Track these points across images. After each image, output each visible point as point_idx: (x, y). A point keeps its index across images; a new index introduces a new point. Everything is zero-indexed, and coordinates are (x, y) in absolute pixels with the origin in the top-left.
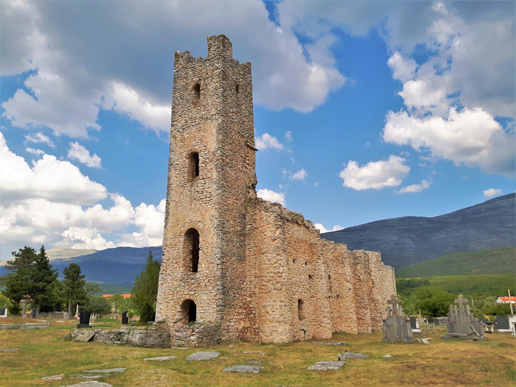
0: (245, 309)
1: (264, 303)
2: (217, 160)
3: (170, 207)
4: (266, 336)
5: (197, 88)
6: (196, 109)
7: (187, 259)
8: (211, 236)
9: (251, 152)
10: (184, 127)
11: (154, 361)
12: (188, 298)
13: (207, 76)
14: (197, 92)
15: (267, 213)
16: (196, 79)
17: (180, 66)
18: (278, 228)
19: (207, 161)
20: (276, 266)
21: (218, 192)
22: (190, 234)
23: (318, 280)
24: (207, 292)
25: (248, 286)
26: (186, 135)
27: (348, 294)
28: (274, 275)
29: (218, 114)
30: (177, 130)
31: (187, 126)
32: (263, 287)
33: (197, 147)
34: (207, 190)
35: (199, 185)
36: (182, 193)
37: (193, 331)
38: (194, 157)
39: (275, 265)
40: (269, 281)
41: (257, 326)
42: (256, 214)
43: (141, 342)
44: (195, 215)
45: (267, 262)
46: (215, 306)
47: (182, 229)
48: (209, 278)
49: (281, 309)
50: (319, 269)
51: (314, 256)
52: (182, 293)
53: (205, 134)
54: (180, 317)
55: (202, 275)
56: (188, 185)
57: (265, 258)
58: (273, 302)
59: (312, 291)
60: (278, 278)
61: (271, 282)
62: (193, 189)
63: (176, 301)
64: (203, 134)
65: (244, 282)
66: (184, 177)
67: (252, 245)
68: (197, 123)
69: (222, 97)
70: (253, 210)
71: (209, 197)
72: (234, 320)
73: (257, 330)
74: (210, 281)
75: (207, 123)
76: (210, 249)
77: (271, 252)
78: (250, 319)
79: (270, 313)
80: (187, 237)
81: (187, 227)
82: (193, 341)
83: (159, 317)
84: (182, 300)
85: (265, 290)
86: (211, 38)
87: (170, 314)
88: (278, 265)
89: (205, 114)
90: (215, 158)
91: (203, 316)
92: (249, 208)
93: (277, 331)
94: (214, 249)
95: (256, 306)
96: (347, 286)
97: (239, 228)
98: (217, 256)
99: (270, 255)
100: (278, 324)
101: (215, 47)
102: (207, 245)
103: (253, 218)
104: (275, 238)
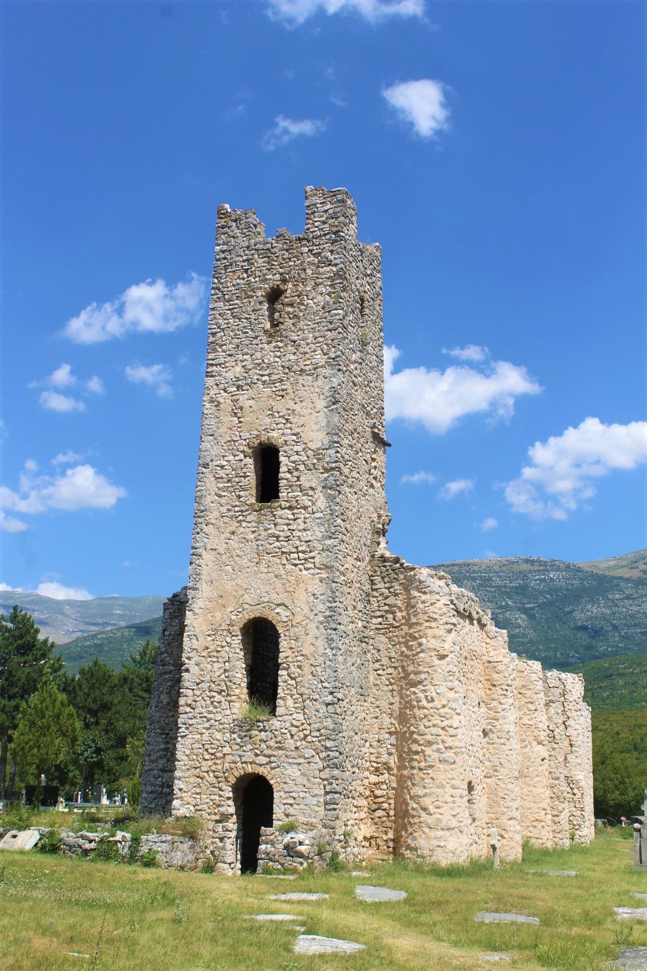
10: (240, 383)
12: (250, 771)
16: (274, 279)
22: (248, 630)
23: (502, 741)
24: (302, 760)
25: (372, 750)
27: (540, 768)
28: (441, 732)
29: (330, 365)
30: (222, 386)
33: (274, 434)
34: (299, 534)
36: (233, 533)
38: (267, 458)
39: (442, 711)
45: (424, 703)
46: (323, 792)
47: (233, 618)
53: (297, 407)
55: (288, 725)
56: (249, 518)
57: (421, 695)
58: (438, 787)
59: (487, 763)
61: (435, 747)
63: (220, 775)
64: (291, 405)
65: (366, 741)
67: (385, 661)
68: (274, 377)
70: (387, 585)
71: (304, 552)
74: (309, 739)
78: (377, 820)
79: (432, 809)
83: (180, 808)
84: (237, 774)
85: (419, 762)
91: (291, 811)
98: (325, 684)
99: (433, 688)
100: (447, 833)
102: (300, 658)
103: (387, 602)
104: (445, 653)
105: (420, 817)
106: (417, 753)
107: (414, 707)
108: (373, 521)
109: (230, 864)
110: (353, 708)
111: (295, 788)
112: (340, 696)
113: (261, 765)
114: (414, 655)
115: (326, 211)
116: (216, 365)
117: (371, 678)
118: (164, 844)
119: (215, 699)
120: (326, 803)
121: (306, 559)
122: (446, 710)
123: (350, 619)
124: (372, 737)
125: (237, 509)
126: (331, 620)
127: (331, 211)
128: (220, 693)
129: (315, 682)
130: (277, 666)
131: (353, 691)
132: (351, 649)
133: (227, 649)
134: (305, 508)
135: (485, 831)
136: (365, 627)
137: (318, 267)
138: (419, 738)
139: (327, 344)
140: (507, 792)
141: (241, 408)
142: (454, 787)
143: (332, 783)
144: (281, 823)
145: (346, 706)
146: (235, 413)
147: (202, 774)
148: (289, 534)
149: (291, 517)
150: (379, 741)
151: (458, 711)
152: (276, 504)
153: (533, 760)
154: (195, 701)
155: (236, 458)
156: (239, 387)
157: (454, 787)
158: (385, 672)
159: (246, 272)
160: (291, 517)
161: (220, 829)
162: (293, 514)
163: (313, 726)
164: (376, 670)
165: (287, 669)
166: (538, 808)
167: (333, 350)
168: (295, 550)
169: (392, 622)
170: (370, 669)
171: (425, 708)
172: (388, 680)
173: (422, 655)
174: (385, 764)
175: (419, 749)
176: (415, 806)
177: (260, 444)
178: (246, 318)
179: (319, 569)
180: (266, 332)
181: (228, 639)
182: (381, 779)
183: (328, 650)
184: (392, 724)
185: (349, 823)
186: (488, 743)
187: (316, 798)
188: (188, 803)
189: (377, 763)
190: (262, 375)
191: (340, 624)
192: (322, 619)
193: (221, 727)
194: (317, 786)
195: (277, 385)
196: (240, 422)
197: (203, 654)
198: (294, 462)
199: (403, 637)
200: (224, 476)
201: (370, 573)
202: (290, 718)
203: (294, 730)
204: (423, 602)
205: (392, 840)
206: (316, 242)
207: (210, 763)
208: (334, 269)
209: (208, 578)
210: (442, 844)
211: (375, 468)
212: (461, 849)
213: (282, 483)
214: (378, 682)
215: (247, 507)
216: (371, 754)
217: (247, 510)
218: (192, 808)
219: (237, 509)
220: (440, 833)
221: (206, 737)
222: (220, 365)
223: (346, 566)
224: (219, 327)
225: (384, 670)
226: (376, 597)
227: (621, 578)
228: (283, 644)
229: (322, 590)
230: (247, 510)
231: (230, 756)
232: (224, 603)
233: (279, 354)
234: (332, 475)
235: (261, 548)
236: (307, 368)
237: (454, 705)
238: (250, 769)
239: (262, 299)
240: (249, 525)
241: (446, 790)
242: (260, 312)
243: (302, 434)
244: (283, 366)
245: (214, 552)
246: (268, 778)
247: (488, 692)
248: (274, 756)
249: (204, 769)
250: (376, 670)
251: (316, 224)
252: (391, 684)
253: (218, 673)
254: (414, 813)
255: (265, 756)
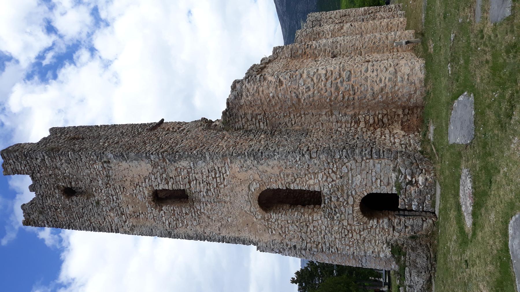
0: (375, 129)
1: (369, 96)
2: (164, 160)
3: (227, 236)
4: (415, 93)
5: (69, 192)
7: (302, 211)
8: (269, 169)
9: (163, 126)
10: (119, 213)
11: (474, 214)
12: (358, 208)
13: (53, 176)
14: (76, 194)
15: (244, 94)
17: (41, 217)
18: (265, 79)
19: (164, 176)
21: (208, 158)
23: (339, 46)
24: (350, 175)
25: (344, 126)
27: (357, 27)
28: (330, 81)
30: (123, 224)
31: (118, 208)
33: (146, 193)
34: (205, 177)
35: (198, 189)
36: (209, 217)
37: (410, 183)
39: (315, 81)
42: (245, 114)
43: (423, 273)
44: (239, 196)
45: (310, 93)
46: (371, 161)
47: (259, 217)
48: (330, 171)
50: (325, 45)
51: (307, 53)
52: (351, 216)
53: (129, 179)
54: (386, 220)
55: (326, 184)
58: (367, 81)
59: (352, 55)
61: (339, 85)
63: (362, 227)
64: (128, 183)
65: (337, 130)
66: (186, 214)
67: (287, 120)
68: (113, 193)
69: (80, 153)
71: (215, 174)
72: (392, 139)
73: (407, 111)
74: (335, 169)
75: (113, 177)
76: (289, 171)
77: (296, 87)
78: (390, 122)
79: (382, 85)
80: (270, 210)
81: (256, 208)
82: (426, 179)
84: (361, 216)
85: (350, 95)
86: (5, 170)
88: (315, 76)
89: (102, 179)
90: (160, 162)
92: (237, 126)
94: (288, 163)
96: (348, 29)
97: (262, 136)
98: (298, 159)
99: (301, 88)
100: (399, 74)
101: (17, 163)
102: (282, 176)
103: (250, 119)
105: (387, 93)
107: (313, 100)
108: (203, 129)
109: (423, 221)
110: (315, 139)
111: (370, 179)
113: (354, 201)
114: (281, 101)
115: (14, 162)
116: (111, 227)
117: (297, 128)
118: (412, 274)
119: (312, 229)
120: (379, 157)
121: (220, 172)
122: (315, 78)
124: (334, 126)
125: (193, 215)
126: (256, 155)
127: (14, 160)
128: (308, 227)
130: (288, 190)
131: (304, 140)
132: (276, 142)
133: (279, 222)
134: (188, 173)
136: (265, 133)
137: (47, 167)
138: (334, 95)
139: (90, 161)
140: (370, 41)
141: (134, 212)
142: (367, 70)
143: (365, 154)
144: (394, 188)
145: (312, 144)
146: (138, 216)
147: (362, 239)
148: (205, 183)
149: (195, 182)
150: (337, 122)
151: (315, 71)
152: (188, 191)
154: (314, 242)
155: (163, 215)
157: (367, 70)
158: (293, 119)
159: (57, 209)
161: (399, 228)
162: (193, 181)
163: (326, 167)
164: (292, 125)
165: (289, 184)
167: (92, 157)
168: (215, 180)
169: (262, 116)
170: (291, 129)
171: (314, 93)
172: (298, 117)
173: (280, 96)
174: (352, 118)
175: (341, 95)
176: (380, 96)
177: (153, 201)
178: (82, 209)
180: (88, 199)
182: (362, 120)
183: (276, 157)
184: (326, 114)
186: (340, 55)
187: (376, 165)
188: (382, 248)
189: (352, 122)
190: (113, 200)
191: (259, 150)
192: (256, 162)
193: (330, 226)
195: (117, 191)
196: (142, 213)
197: (284, 236)
198: (162, 180)
199: (270, 109)
200: (175, 222)
202: (321, 182)
203: (329, 180)
204: (247, 96)
205: (403, 111)
207: (355, 234)
209: (237, 233)
210: (406, 77)
211: (173, 128)
212: (410, 64)
214: (300, 124)
215: (192, 209)
216: (346, 127)
217: (193, 208)
219: (193, 215)
220: (399, 79)
222: (111, 225)
223: (224, 146)
225: (292, 120)
226: (248, 126)
227: (289, 26)
228: (274, 186)
229: (238, 162)
230: (193, 208)
231: (349, 221)
232: (251, 223)
233: (100, 190)
234: (166, 156)
235: (215, 200)
236: (105, 173)
237: (312, 73)
238: (357, 208)
239: (70, 200)
240: (202, 207)
242: (78, 201)
243: (144, 176)
244: (106, 188)
245: (221, 229)
246: (363, 196)
247: (309, 56)
248: (348, 192)
250: (292, 125)
252: (300, 115)
253: (295, 227)
254: (385, 97)
255: (348, 197)
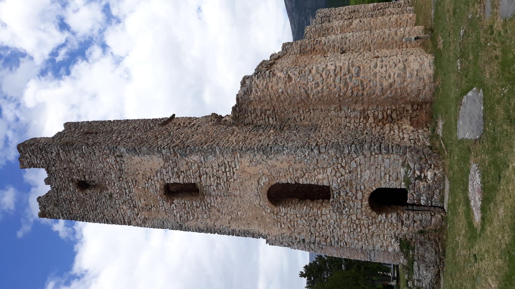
0: (384, 124)
1: (378, 92)
2: (175, 155)
3: (237, 229)
4: (424, 88)
5: (83, 185)
6: (108, 187)
8: (278, 164)
9: (174, 121)
10: (132, 206)
11: (483, 209)
12: (367, 202)
13: (68, 169)
15: (253, 89)
16: (72, 187)
17: (56, 209)
18: (274, 75)
19: (175, 170)
20: (326, 74)
21: (218, 152)
23: (348, 42)
25: (352, 121)
26: (142, 203)
27: (366, 23)
28: (339, 77)
29: (114, 153)
30: (135, 217)
31: (130, 201)
32: (355, 93)
33: (158, 186)
36: (219, 211)
37: (419, 177)
39: (324, 76)
40: (346, 84)
41: (409, 108)
42: (255, 110)
44: (249, 190)
45: (319, 89)
46: (380, 156)
47: (269, 211)
48: (339, 166)
49: (386, 66)
51: (316, 49)
52: (359, 211)
53: (141, 173)
54: (395, 215)
55: (335, 178)
56: (209, 201)
58: (376, 77)
59: (362, 50)
60: (343, 70)
61: (348, 80)
62: (214, 193)
63: (370, 221)
64: (140, 176)
65: (346, 126)
66: (197, 207)
67: (296, 115)
68: (126, 186)
69: (93, 147)
71: (225, 168)
73: (415, 106)
75: (126, 171)
76: (298, 166)
77: (306, 82)
79: (391, 81)
81: (265, 202)
84: (370, 211)
85: (359, 90)
87: (389, 232)
88: (324, 72)
89: (115, 173)
93: (417, 71)
94: (297, 158)
95: (381, 108)
96: (357, 25)
97: (272, 131)
98: (307, 154)
99: (310, 84)
100: (408, 70)
102: (291, 170)
103: (259, 114)
106: (352, 93)
107: (322, 95)
108: (213, 124)
110: (324, 135)
111: (378, 173)
112: (314, 144)
113: (363, 196)
114: (290, 97)
115: (30, 156)
116: (124, 220)
117: (306, 123)
118: (421, 268)
119: (321, 223)
121: (230, 167)
122: (324, 74)
123: (267, 138)
124: (343, 121)
125: (204, 208)
126: (265, 150)
127: (30, 154)
129: (306, 160)
131: (312, 135)
132: (285, 137)
133: (288, 216)
134: (199, 167)
135: (404, 49)
137: (62, 161)
138: (343, 91)
140: (380, 37)
141: (146, 205)
142: (376, 66)
143: (374, 149)
145: (321, 139)
146: (149, 209)
147: (371, 233)
148: (215, 177)
150: (346, 117)
151: (324, 66)
152: (199, 185)
153: (361, 27)
154: (323, 236)
156: (135, 207)
157: (376, 66)
159: (71, 202)
160: (205, 176)
161: (408, 223)
162: (204, 175)
163: (335, 162)
164: (301, 120)
166: (389, 22)
167: (105, 151)
168: (225, 174)
169: (271, 111)
171: (323, 88)
172: (307, 112)
173: (289, 91)
174: (361, 113)
176: (389, 92)
177: (165, 194)
178: (96, 202)
179: (234, 159)
181: (282, 214)
182: (371, 115)
183: (285, 152)
184: (335, 109)
185: (402, 136)
186: (349, 50)
187: (385, 160)
188: (391, 242)
190: (126, 193)
191: (268, 145)
192: (265, 156)
193: (338, 220)
194: (376, 160)
196: (154, 206)
198: (173, 174)
199: (279, 104)
200: (186, 215)
201: (243, 125)
202: (330, 176)
203: (338, 174)
206: (48, 162)
207: (363, 228)
208: (61, 151)
209: (246, 226)
210: (415, 73)
212: (419, 60)
213: (186, 181)
214: (309, 119)
215: (202, 202)
216: (355, 122)
217: (204, 202)
218: (394, 240)
219: (204, 208)
220: (408, 74)
221: (346, 230)
222: (124, 218)
224: (103, 218)
225: (300, 116)
226: (257, 121)
227: (298, 22)
228: (283, 181)
229: (248, 157)
230: (204, 202)
231: (358, 215)
232: (260, 217)
233: (112, 184)
234: (177, 151)
235: (226, 194)
236: (118, 167)
237: (321, 69)
238: (366, 203)
240: (213, 201)
241: (377, 72)
243: (156, 170)
244: (119, 181)
245: (231, 222)
246: (372, 191)
247: (318, 52)
248: (356, 187)
249: (367, 232)
250: (301, 120)
251: (39, 162)
252: (309, 111)
253: (304, 221)
254: (394, 92)
255: (357, 192)
